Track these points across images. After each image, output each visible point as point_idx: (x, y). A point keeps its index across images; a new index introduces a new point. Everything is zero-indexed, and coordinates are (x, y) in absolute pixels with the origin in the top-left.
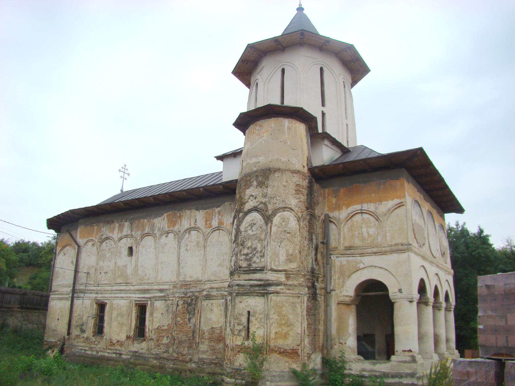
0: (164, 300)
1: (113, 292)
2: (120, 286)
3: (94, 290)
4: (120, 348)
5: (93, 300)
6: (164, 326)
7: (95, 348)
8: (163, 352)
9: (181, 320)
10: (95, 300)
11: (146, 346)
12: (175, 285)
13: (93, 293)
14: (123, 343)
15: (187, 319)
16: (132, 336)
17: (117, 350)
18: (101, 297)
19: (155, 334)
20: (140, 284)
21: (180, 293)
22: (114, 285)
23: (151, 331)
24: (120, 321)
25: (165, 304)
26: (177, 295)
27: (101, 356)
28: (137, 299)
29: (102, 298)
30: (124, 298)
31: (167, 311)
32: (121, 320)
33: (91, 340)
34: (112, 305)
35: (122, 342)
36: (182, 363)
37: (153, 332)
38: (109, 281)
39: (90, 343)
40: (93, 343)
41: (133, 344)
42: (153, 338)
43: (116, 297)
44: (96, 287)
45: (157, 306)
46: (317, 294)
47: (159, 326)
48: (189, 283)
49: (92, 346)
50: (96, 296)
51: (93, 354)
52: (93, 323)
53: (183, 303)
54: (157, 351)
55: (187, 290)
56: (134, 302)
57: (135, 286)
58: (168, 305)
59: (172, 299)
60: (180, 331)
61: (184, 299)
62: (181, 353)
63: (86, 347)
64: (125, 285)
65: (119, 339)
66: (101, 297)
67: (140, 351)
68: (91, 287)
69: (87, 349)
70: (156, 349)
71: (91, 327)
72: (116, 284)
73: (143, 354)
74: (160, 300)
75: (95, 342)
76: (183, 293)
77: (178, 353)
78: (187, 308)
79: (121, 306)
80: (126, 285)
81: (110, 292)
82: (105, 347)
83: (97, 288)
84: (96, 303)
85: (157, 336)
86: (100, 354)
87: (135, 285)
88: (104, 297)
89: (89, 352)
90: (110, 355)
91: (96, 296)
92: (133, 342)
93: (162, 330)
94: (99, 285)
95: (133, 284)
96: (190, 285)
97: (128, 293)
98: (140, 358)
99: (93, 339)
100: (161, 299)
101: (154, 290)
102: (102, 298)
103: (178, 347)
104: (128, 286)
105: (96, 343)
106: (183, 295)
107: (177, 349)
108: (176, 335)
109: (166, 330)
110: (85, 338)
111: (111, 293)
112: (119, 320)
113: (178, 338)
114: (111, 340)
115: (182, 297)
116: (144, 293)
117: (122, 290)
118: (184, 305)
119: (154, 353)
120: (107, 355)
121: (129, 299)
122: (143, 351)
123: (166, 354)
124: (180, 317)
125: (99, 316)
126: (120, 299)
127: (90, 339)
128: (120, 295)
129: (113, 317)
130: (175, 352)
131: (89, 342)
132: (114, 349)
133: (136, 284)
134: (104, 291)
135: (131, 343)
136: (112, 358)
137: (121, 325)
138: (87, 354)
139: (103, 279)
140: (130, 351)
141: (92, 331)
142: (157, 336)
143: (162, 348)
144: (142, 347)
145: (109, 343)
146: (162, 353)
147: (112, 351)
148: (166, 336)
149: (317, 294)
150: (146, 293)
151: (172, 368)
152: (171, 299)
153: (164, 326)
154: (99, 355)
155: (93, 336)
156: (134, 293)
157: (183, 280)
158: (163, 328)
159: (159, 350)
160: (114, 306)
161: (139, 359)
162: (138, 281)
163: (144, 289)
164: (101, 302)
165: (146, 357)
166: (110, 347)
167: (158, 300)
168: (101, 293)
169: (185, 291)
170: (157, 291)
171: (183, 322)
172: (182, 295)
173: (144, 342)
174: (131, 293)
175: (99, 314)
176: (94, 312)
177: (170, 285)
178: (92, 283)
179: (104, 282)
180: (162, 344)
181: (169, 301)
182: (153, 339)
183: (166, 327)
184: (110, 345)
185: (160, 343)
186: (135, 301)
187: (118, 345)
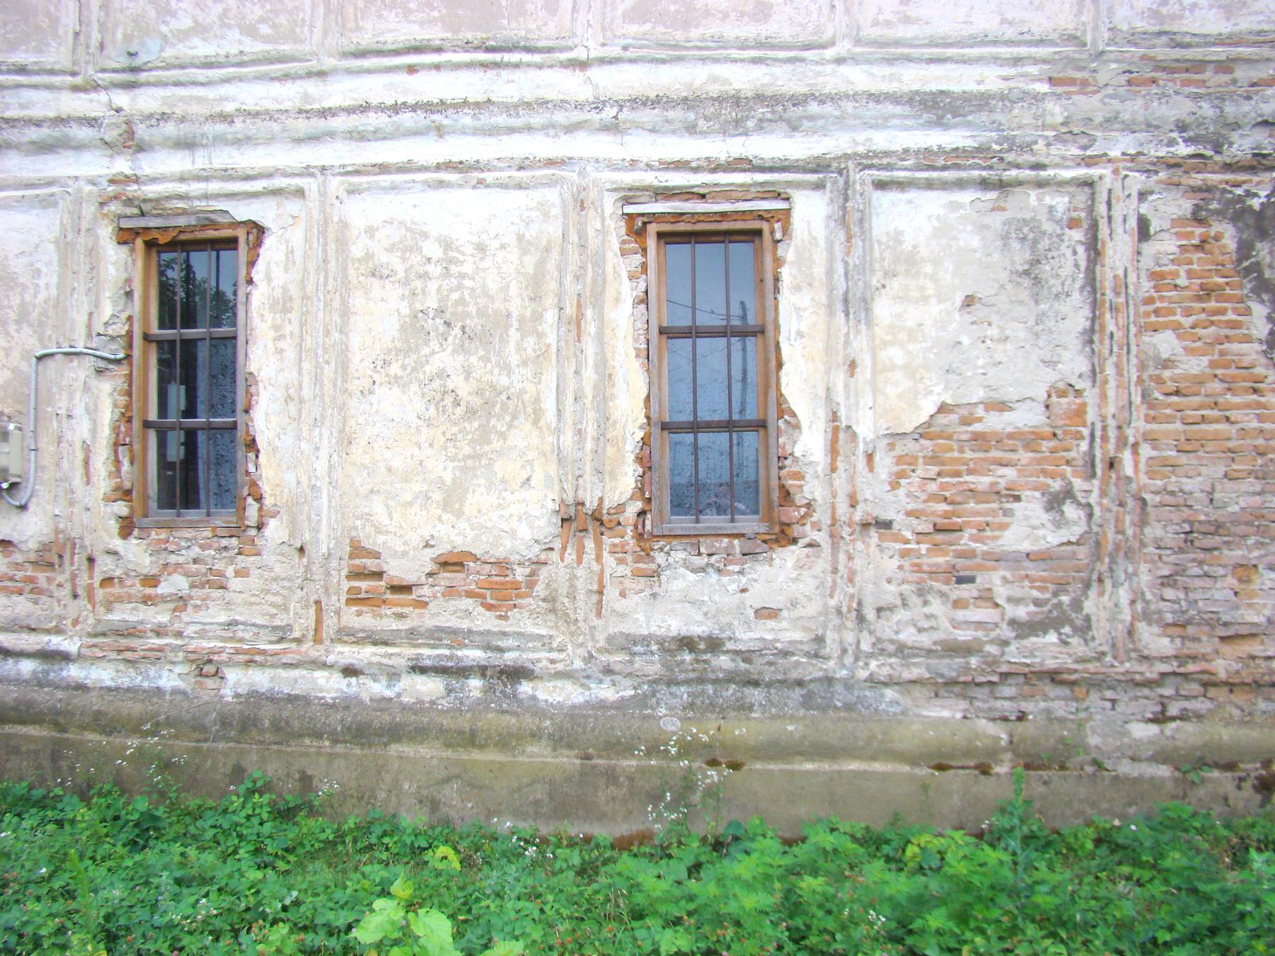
0: (984, 184)
1: (340, 123)
2: (412, 69)
3: (92, 122)
4: (484, 621)
5: (89, 210)
6: (1002, 406)
7: (159, 632)
8: (1013, 623)
9: (1189, 351)
10: (114, 207)
11: (808, 585)
12: (1070, 62)
13: (80, 147)
14: (520, 574)
15: (1248, 339)
16: (621, 508)
17: (458, 637)
18: (182, 179)
19: (901, 475)
20: (663, 54)
21: (1149, 126)
22: (329, 63)
23: (870, 457)
24: (457, 382)
25: (997, 220)
26: (1121, 145)
27: (254, 697)
28: (650, 178)
29: (196, 188)
30: (489, 177)
31: (1031, 273)
32: (468, 374)
33: (105, 565)
34: (342, 244)
35: (503, 565)
36: (1239, 698)
37: (885, 464)
38: (266, 39)
39: (100, 594)
40: (138, 589)
41: (655, 574)
42: (886, 515)
43: (383, 169)
44: (103, 97)
45: (897, 237)
46: (696, 434)
47: (943, 409)
48: (1220, 53)
49: (122, 615)
50: (122, 165)
51: (159, 691)
52: (107, 415)
53: (1197, 208)
54: (944, 623)
55: (1230, 109)
56: (610, 204)
57: (595, 73)
58: (1033, 224)
59: (1081, 172)
60: (1187, 446)
61: (1197, 179)
62: (1213, 622)
63: (58, 631)
64: (470, 65)
65: (455, 537)
66: (182, 179)
67: (748, 635)
68: (44, 95)
69: (70, 645)
70: (936, 606)
71: (87, 450)
72: (362, 54)
73: (785, 654)
74: (929, 185)
75: (151, 581)
76: (1182, 127)
77: (1179, 626)
78: (1245, 249)
79: (447, 245)
80: (484, 66)
81: (303, 126)
82: (303, 622)
83: (122, 99)
84: (126, 236)
85: (933, 497)
86: (237, 681)
87: (602, 61)
88: (227, 175)
89: (103, 675)
90: (377, 688)
91: (122, 165)
92: (647, 555)
93: (977, 437)
94: (143, 76)
95: (580, 54)
96: (1224, 66)
97: (529, 128)
98: (755, 695)
99: (137, 553)
100: (947, 175)
101: (855, 97)
102: (196, 188)
103: (1180, 570)
104: (505, 74)
105: (174, 584)
106: (1183, 150)
107: (1169, 593)
108: (1151, 474)
109: (1030, 439)
110: (32, 545)
111: (314, 138)
112: (442, 374)
113: (1179, 502)
114: (358, 550)
115: (1173, 165)
116: (737, 127)
117: (442, 106)
118: (1199, 231)
119: (908, 636)
120: (329, 685)
121: (552, 183)
122: (786, 632)
123: (1052, 637)
124: (1176, 327)
125: (160, 343)
126: (441, 184)
127: (91, 560)
128: (428, 150)
129: (355, 341)
130: (1147, 616)
131: (83, 580)
132: (412, 635)
133: (615, 51)
134: (226, 118)
135: (622, 570)
136: (405, 708)
137: (471, 413)
138: (81, 687)
139: (185, 23)
140: (628, 644)
141: (103, 483)
142: (933, 497)
143: (1001, 593)
144: (757, 597)
145: (346, 585)
146: (1007, 633)
147: (402, 654)
148: (1044, 490)
149: (696, 434)
150: (761, 126)
151: (1161, 757)
152: (1067, 174)
153: (1002, 406)
154: (228, 693)
155: (127, 527)
156: (613, 128)
157: (1140, 25)
158: (994, 422)
159: (961, 615)
160: (357, 250)
161: (745, 707)
162: (634, 29)
163: (714, 90)
164: (182, 221)
165: (829, 680)
166: (366, 620)
167: (901, 185)
168: (187, 144)
169: (1207, 110)
170: (890, 108)
171: (1212, 365)
172: (1171, 143)
173: (788, 557)
174: (571, 129)
175: (155, 330)
176: (107, 310)
177: (1017, 61)
178: (57, 55)
179: (202, 49)
180: (997, 559)
181: (1033, 194)
182: (887, 525)
183: (1028, 417)
184: (355, 599)
185: (968, 554)
186: (629, 195)
187: (451, 592)
